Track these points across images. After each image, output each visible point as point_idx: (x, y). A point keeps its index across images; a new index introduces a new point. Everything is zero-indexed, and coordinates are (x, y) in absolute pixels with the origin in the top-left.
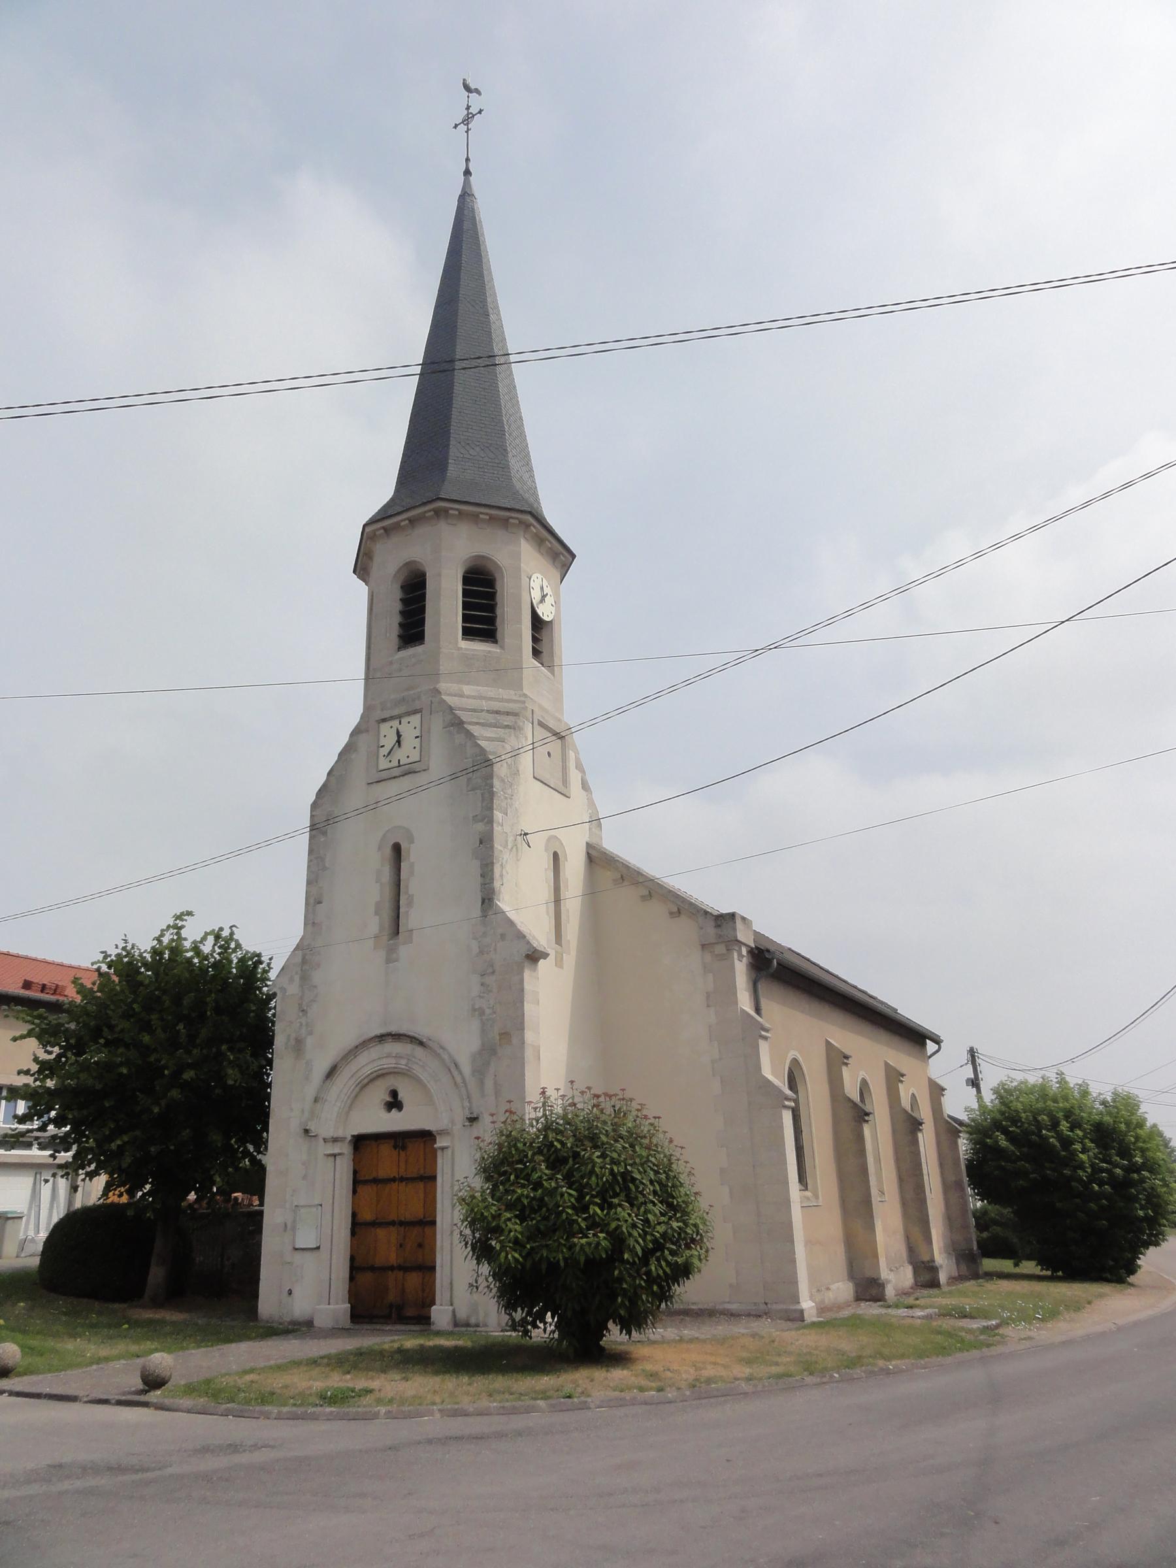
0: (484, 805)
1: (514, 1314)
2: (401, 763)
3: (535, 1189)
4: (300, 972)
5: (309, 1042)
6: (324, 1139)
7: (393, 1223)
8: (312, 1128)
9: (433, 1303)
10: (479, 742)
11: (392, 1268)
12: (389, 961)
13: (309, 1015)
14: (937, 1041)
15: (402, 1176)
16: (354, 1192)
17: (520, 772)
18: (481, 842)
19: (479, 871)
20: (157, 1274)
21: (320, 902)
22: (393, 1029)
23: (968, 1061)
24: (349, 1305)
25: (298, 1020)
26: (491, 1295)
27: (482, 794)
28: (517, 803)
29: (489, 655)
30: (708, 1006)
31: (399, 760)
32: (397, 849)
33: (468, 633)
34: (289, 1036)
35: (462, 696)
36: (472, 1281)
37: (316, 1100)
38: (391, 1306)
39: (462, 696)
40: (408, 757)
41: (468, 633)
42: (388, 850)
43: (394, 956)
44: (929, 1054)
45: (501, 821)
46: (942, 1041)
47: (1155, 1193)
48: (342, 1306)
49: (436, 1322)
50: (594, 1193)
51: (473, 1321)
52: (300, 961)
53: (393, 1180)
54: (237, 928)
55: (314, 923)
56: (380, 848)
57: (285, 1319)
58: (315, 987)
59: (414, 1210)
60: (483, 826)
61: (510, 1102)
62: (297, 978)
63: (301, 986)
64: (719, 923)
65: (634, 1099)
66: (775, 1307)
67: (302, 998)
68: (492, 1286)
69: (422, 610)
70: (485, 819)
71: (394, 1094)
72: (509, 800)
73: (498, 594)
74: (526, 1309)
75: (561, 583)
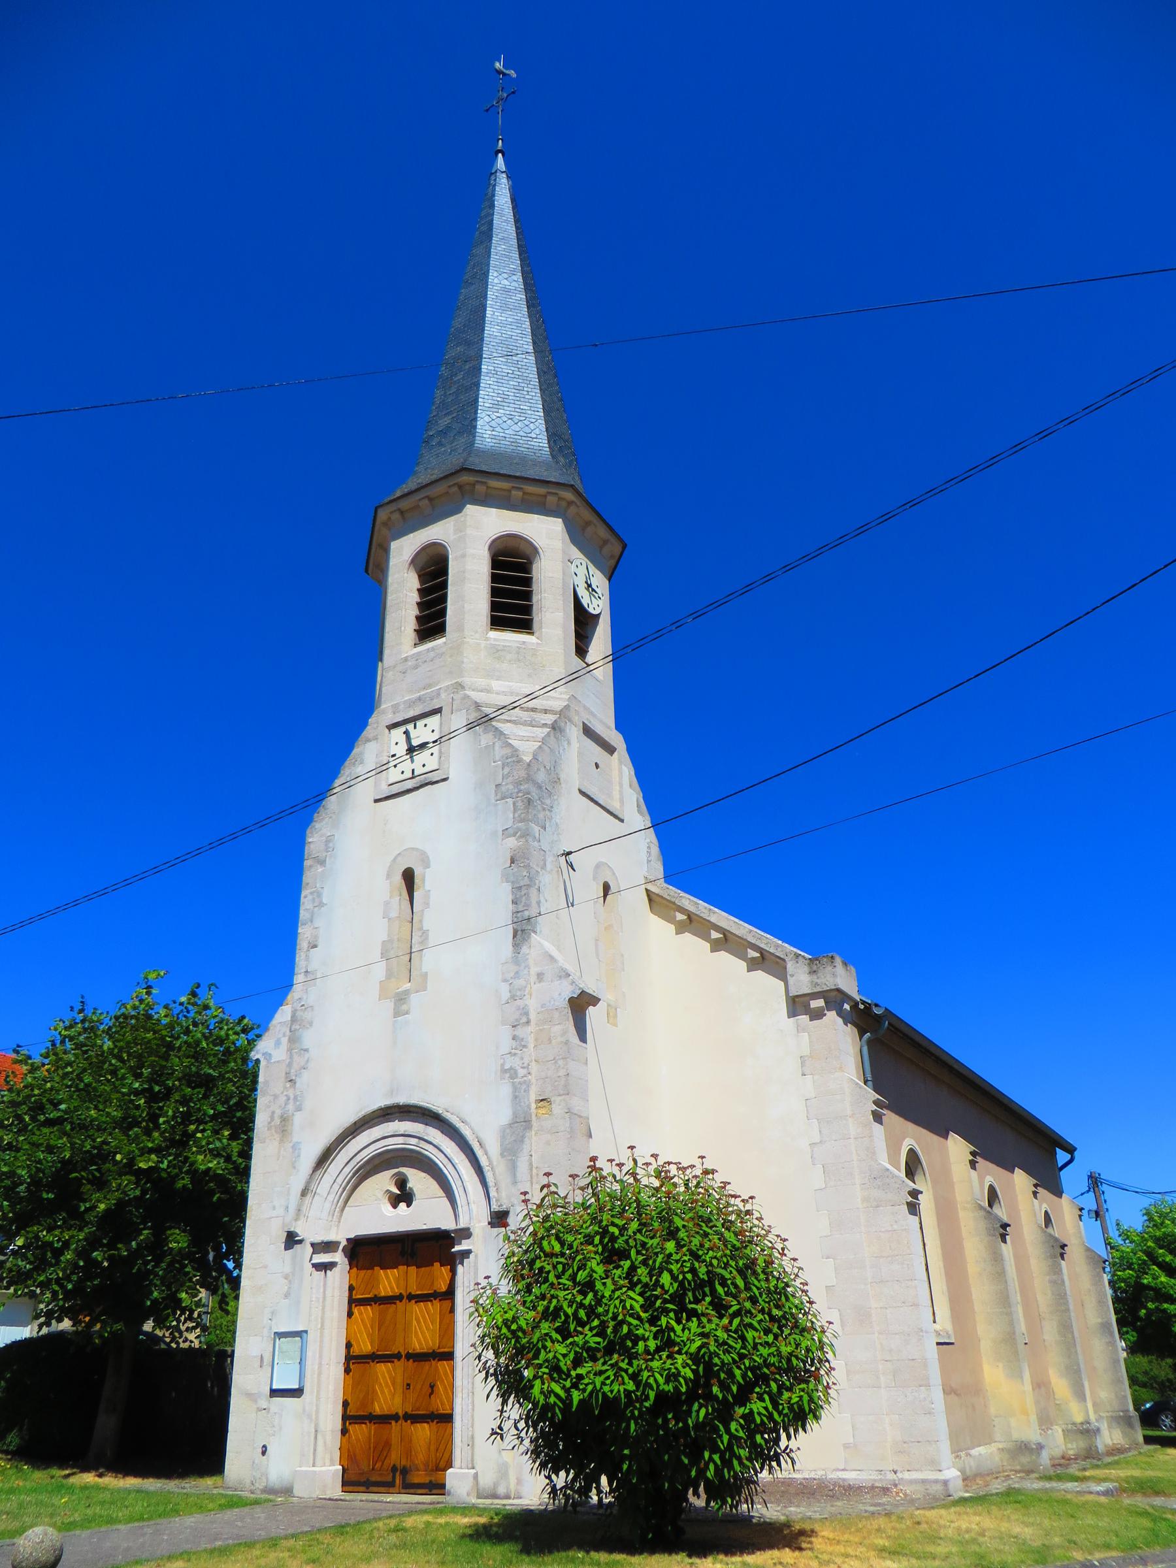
0: (516, 815)
1: (554, 1477)
2: (416, 774)
3: (583, 1293)
4: (288, 1033)
5: (298, 1119)
6: (313, 1245)
7: (398, 1356)
8: (298, 1231)
9: (449, 1465)
10: (510, 741)
11: (396, 1417)
12: (397, 1014)
13: (298, 1085)
14: (1070, 1150)
15: (410, 1293)
16: (350, 1314)
17: (561, 779)
18: (512, 861)
19: (510, 898)
20: (106, 1424)
21: (315, 946)
22: (402, 1099)
23: (1090, 1188)
24: (341, 1467)
25: (285, 1093)
26: (523, 1449)
27: (514, 804)
28: (558, 817)
29: (524, 646)
30: (804, 1075)
31: (413, 770)
32: (409, 877)
33: (497, 622)
34: (273, 1113)
35: (488, 691)
36: (495, 1425)
37: (304, 1193)
38: (394, 1469)
39: (488, 691)
40: (424, 765)
41: (497, 622)
42: (398, 879)
43: (404, 1007)
44: (1059, 1166)
45: (537, 835)
46: (1075, 1149)
47: (755, 1478)
48: (331, 1468)
49: (452, 1491)
50: (666, 1296)
51: (501, 1490)
52: (289, 1019)
53: (400, 1298)
54: (217, 988)
55: (307, 972)
56: (388, 876)
57: (257, 1485)
58: (306, 1050)
59: (422, 1338)
60: (516, 842)
61: (548, 1174)
62: (285, 1040)
63: (290, 1050)
64: (815, 968)
65: (717, 1171)
66: (907, 1476)
67: (290, 1065)
68: (523, 1434)
69: (443, 599)
70: (517, 833)
71: (402, 1183)
72: (547, 812)
73: (534, 608)
74: (572, 1471)
75: (583, 1037)
